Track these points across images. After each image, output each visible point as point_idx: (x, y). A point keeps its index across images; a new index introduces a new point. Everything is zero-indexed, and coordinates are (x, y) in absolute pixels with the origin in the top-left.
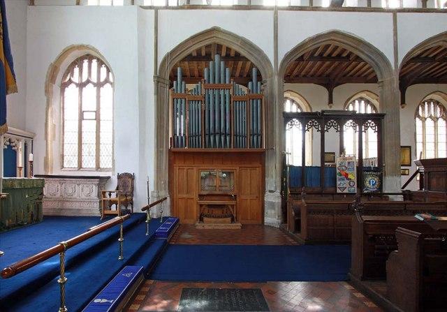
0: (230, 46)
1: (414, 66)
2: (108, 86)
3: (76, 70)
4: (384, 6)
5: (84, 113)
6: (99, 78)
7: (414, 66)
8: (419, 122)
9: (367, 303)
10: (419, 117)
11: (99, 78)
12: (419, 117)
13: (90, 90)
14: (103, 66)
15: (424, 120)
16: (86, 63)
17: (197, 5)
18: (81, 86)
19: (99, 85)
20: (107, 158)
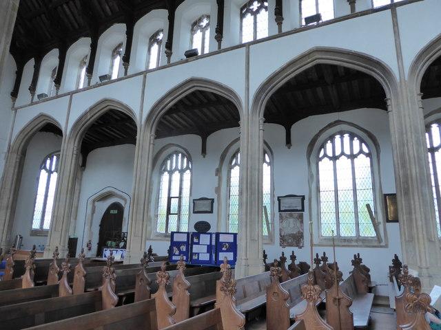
0: (422, 116)
1: (201, 97)
2: (188, 171)
3: (169, 162)
4: (377, 5)
5: (172, 199)
6: (171, 166)
7: (201, 97)
8: (43, 174)
9: (56, 275)
10: (45, 168)
11: (171, 166)
12: (45, 168)
13: (344, 163)
14: (356, 138)
15: (50, 172)
16: (338, 138)
17: (396, 14)
18: (334, 158)
19: (352, 157)
20: (367, 181)
